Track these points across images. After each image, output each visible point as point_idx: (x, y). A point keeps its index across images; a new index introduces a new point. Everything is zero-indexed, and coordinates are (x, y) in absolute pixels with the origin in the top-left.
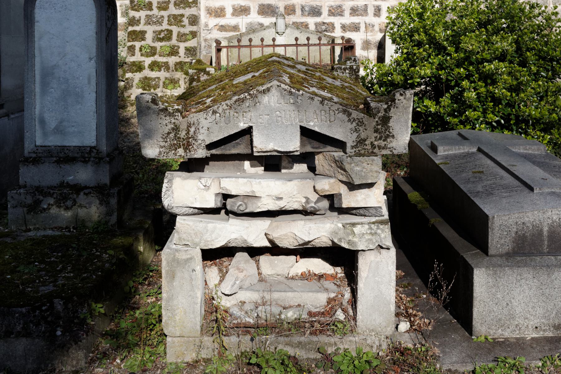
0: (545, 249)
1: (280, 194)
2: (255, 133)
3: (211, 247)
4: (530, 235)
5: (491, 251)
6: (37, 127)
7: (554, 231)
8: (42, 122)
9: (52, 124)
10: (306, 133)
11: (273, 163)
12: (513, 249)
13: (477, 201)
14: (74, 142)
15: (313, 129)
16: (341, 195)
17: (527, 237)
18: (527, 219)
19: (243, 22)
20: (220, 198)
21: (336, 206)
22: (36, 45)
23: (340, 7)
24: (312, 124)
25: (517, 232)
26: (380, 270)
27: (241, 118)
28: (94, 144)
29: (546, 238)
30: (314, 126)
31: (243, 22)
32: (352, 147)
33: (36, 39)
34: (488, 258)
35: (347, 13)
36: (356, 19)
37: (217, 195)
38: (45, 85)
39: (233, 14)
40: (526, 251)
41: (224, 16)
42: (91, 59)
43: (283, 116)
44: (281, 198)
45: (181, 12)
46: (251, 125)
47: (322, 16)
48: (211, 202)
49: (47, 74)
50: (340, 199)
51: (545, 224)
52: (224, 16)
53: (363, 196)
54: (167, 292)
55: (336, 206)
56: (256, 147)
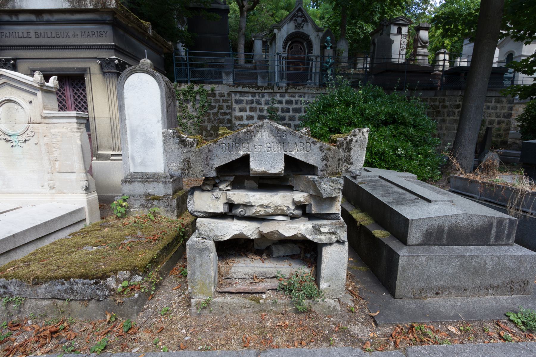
1: (269, 204)
2: (251, 159)
3: (220, 240)
5: (410, 242)
6: (130, 162)
7: (451, 230)
8: (133, 158)
9: (138, 160)
10: (289, 161)
11: (267, 183)
13: (397, 208)
14: (151, 170)
15: (294, 157)
16: (311, 205)
20: (227, 206)
21: (307, 212)
22: (126, 113)
23: (294, 116)
24: (293, 153)
25: (427, 230)
26: (336, 259)
27: (241, 148)
28: (163, 172)
29: (445, 234)
30: (295, 154)
32: (321, 171)
33: (126, 109)
34: (405, 247)
35: (297, 119)
36: (251, 114)
37: (225, 203)
38: (133, 137)
39: (246, 119)
40: (432, 243)
41: (243, 120)
42: (159, 121)
43: (272, 146)
46: (248, 153)
48: (220, 208)
49: (134, 132)
50: (311, 208)
51: (447, 225)
52: (243, 120)
53: (327, 206)
54: (191, 270)
55: (307, 212)
56: (252, 170)
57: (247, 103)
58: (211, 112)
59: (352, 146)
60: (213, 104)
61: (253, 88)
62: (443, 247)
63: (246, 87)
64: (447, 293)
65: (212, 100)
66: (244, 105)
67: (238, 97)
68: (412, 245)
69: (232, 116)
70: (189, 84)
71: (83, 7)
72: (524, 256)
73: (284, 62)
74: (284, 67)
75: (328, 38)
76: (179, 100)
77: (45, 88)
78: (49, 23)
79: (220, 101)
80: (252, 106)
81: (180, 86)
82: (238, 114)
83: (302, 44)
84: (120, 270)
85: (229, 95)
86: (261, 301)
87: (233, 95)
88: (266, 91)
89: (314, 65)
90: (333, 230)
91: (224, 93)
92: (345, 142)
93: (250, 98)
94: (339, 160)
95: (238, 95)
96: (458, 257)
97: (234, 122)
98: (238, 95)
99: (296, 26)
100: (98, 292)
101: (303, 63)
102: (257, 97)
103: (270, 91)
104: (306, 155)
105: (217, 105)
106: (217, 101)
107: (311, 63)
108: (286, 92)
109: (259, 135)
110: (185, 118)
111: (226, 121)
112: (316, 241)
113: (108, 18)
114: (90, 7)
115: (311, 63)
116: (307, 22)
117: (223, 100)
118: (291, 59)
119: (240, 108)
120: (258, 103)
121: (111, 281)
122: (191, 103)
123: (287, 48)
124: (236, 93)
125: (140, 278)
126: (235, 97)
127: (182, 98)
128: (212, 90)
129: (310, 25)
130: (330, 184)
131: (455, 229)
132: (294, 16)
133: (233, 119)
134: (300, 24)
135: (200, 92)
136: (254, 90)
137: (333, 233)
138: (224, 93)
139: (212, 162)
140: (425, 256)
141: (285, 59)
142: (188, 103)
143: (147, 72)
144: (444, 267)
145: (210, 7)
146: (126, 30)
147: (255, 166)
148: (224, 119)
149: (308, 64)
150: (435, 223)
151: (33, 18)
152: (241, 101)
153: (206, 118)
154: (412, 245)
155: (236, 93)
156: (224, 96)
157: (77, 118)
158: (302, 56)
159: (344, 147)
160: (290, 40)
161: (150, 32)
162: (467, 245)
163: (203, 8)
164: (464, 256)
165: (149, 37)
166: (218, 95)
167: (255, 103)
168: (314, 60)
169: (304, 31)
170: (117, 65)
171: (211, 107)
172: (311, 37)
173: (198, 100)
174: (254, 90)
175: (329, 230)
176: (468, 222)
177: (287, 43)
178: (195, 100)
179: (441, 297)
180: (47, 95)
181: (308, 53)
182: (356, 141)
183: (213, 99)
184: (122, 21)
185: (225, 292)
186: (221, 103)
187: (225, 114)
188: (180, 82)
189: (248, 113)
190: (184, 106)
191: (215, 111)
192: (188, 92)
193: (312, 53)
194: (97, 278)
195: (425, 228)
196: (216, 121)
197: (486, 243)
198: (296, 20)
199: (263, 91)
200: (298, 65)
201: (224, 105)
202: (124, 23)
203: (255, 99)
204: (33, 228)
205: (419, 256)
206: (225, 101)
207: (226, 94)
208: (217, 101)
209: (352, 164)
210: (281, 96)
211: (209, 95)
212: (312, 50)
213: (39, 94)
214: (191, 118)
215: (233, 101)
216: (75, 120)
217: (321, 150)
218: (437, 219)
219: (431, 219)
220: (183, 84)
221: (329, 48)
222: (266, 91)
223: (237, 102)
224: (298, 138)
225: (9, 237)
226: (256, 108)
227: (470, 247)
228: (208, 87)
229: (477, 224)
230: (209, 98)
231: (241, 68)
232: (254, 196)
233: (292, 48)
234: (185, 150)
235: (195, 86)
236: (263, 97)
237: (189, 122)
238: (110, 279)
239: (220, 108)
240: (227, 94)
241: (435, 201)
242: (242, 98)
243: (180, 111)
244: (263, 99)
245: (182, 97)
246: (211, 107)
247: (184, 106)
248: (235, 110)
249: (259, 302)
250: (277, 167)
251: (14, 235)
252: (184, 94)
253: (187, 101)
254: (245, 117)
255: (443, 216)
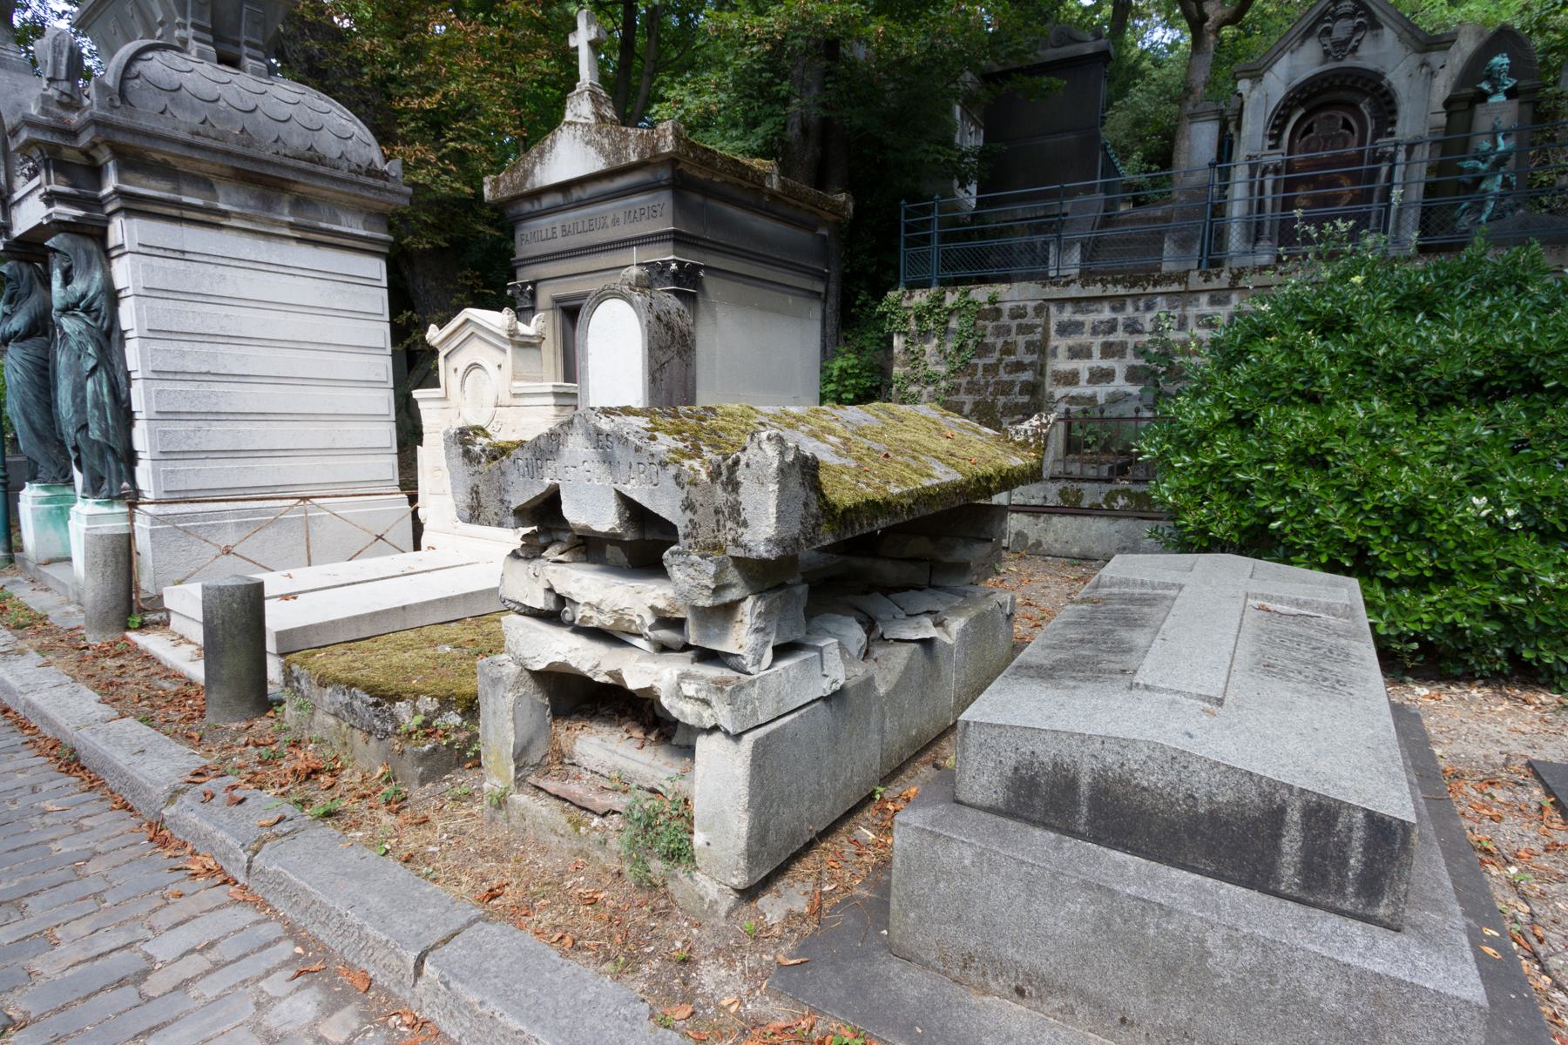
0: (1081, 824)
4: (1047, 783)
7: (1106, 792)
12: (1008, 803)
17: (1038, 785)
18: (1043, 747)
19: (1102, 391)
24: (628, 487)
25: (1016, 769)
31: (1102, 391)
32: (686, 536)
36: (1106, 364)
39: (1089, 381)
44: (1191, 736)
45: (1012, 377)
47: (1116, 383)
48: (540, 601)
57: (1095, 331)
58: (981, 362)
59: (741, 474)
60: (989, 340)
61: (1115, 282)
62: (1069, 842)
63: (1095, 282)
64: (1057, 1002)
65: (989, 329)
66: (1084, 338)
67: (1068, 314)
68: (971, 806)
69: (1042, 373)
70: (933, 290)
71: (624, 163)
72: (1399, 983)
73: (1269, 184)
74: (1268, 202)
75: (1497, 60)
76: (906, 334)
77: (517, 339)
78: (581, 204)
79: (1009, 331)
80: (1111, 338)
81: (911, 297)
82: (1062, 364)
83: (1353, 107)
84: (426, 693)
85: (1041, 310)
86: (582, 829)
87: (1053, 309)
88: (1158, 289)
89: (1398, 178)
90: (702, 695)
91: (1025, 307)
92: (723, 468)
93: (1106, 314)
94: (717, 512)
95: (1069, 308)
96: (1086, 886)
97: (1049, 389)
98: (1069, 308)
99: (1327, 53)
100: (377, 722)
101: (1355, 178)
102: (1130, 309)
103: (1175, 287)
104: (651, 494)
105: (1000, 343)
106: (1002, 331)
107: (1384, 170)
108: (1233, 287)
109: (571, 439)
110: (916, 381)
111: (1017, 389)
112: (675, 714)
113: (664, 174)
114: (634, 158)
115: (1384, 170)
116: (1375, 25)
117: (1019, 326)
118: (1302, 169)
119: (1070, 349)
120: (1133, 328)
121: (402, 708)
122: (936, 341)
123: (1287, 135)
124: (1061, 302)
125: (458, 720)
126: (1057, 316)
127: (914, 328)
128: (992, 301)
129: (1388, 35)
130: (691, 571)
131: (1120, 790)
132: (1320, 19)
133: (1048, 380)
134: (1348, 41)
135: (959, 309)
136: (1121, 290)
137: (706, 702)
138: (1025, 307)
139: (507, 498)
140: (970, 845)
141: (1277, 171)
142: (927, 341)
143: (622, 296)
144: (1039, 906)
145: (1037, 61)
146: (707, 190)
147: (573, 512)
148: (1012, 383)
149: (1373, 175)
150: (1046, 752)
151: (558, 199)
152: (1077, 327)
153: (964, 381)
154: (971, 806)
155: (1061, 302)
156: (1023, 316)
157: (556, 394)
158: (1352, 149)
159: (724, 478)
160: (1302, 103)
161: (774, 183)
162: (1160, 860)
163: (1017, 70)
164: (1112, 893)
165: (773, 196)
166: (1006, 313)
167: (1120, 328)
168: (1401, 157)
169: (1358, 64)
170: (675, 274)
171: (983, 349)
172: (1389, 77)
173: (954, 331)
174: (1121, 290)
175: (697, 691)
176: (1172, 777)
177: (1287, 119)
178: (946, 331)
179: (1037, 1009)
180: (523, 351)
181: (1376, 135)
182: (748, 465)
183: (990, 325)
184: (697, 173)
185: (541, 789)
186: (1013, 337)
187: (1019, 367)
188: (912, 286)
189: (1097, 362)
190: (916, 349)
191: (991, 359)
192: (930, 311)
193: (1392, 134)
194: (382, 697)
195: (1010, 760)
196: (991, 389)
197: (1260, 878)
198: (1328, 32)
199: (1150, 289)
200: (1332, 182)
201: (1021, 340)
202: (702, 176)
203: (1121, 317)
204: (440, 600)
205: (952, 839)
206: (1025, 329)
207: (1030, 311)
208: (1002, 331)
209: (745, 524)
210: (1213, 301)
211: (982, 315)
212: (1393, 123)
213: (509, 349)
214: (931, 380)
215: (1053, 327)
216: (551, 400)
217: (678, 484)
218: (1048, 737)
219: (1028, 734)
220: (918, 292)
221: (1501, 98)
222: (1158, 289)
223: (1064, 329)
224: (632, 452)
225: (396, 609)
226: (1123, 345)
227: (1176, 873)
228: (981, 294)
229: (1210, 797)
230: (980, 323)
231: (1125, 222)
232: (578, 580)
233: (1309, 130)
234: (472, 470)
235: (948, 294)
236: (1149, 308)
237: (925, 392)
238: (403, 704)
239: (1008, 349)
240: (1036, 309)
241: (1147, 687)
242: (1079, 317)
243: (904, 364)
244: (1149, 316)
245: (913, 326)
246: (983, 349)
247: (916, 349)
248: (1054, 355)
249: (577, 830)
250: (604, 519)
251: (404, 608)
252: (919, 318)
253: (925, 335)
254: (1085, 375)
255: (1072, 735)
